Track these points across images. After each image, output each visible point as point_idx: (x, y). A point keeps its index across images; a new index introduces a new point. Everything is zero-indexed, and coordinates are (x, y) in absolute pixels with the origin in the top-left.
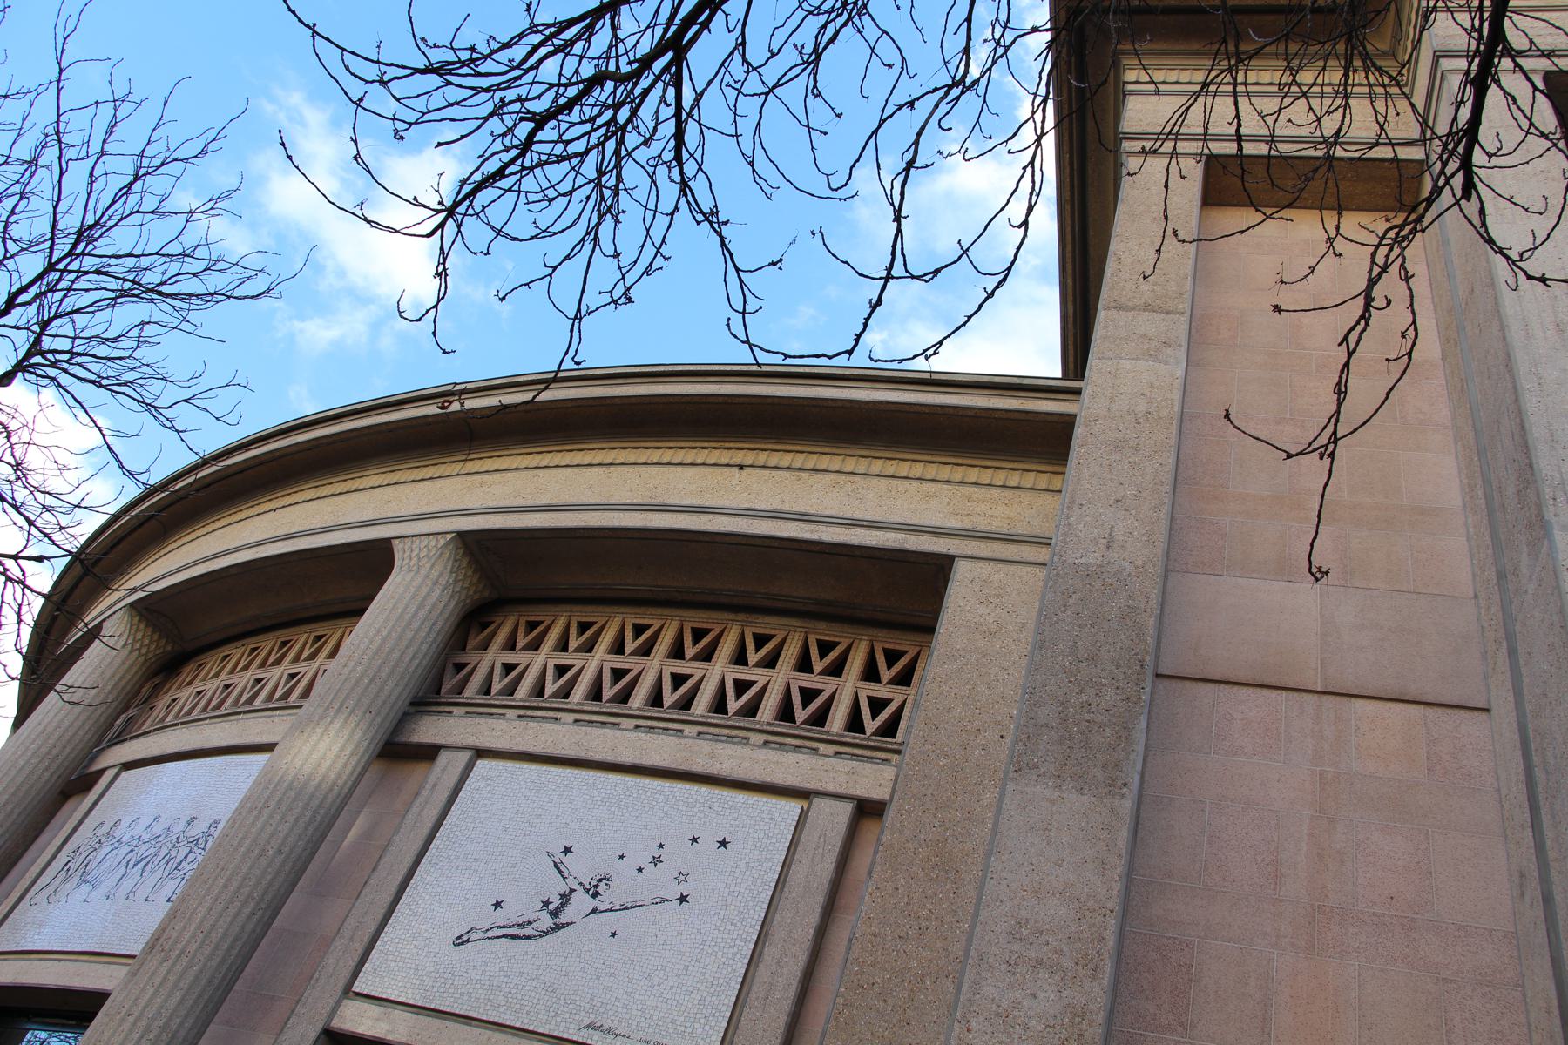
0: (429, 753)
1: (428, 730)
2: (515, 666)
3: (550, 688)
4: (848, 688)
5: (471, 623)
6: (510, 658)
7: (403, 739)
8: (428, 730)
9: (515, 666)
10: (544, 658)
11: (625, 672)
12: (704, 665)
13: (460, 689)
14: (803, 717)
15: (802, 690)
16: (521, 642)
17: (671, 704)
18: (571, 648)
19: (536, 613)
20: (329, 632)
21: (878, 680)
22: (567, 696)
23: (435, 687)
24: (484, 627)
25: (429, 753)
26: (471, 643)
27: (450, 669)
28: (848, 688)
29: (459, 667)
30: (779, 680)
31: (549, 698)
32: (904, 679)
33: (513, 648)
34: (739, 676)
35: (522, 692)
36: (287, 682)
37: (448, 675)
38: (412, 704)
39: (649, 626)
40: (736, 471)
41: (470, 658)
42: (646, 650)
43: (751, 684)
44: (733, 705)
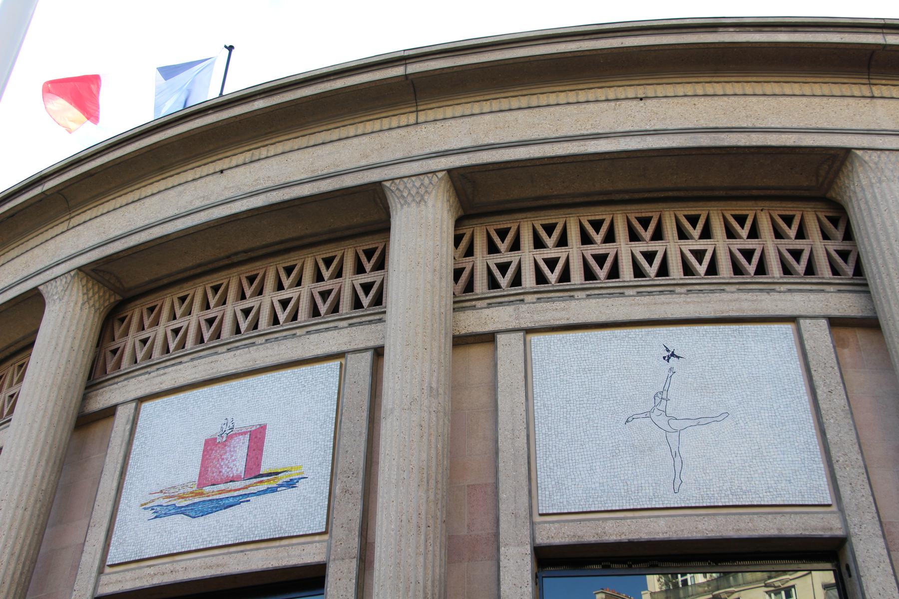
0: (110, 412)
1: (103, 399)
2: (147, 339)
3: (243, 326)
4: (350, 281)
5: (111, 321)
6: (175, 324)
7: (86, 411)
8: (103, 399)
9: (147, 339)
10: (165, 327)
11: (329, 292)
12: (188, 317)
13: (118, 366)
14: (327, 307)
15: (281, 302)
16: (147, 323)
17: (249, 328)
18: (212, 305)
19: (149, 301)
20: (191, 292)
21: (365, 272)
22: (219, 337)
23: (99, 368)
24: (122, 320)
25: (110, 412)
26: (117, 334)
27: (109, 354)
28: (350, 281)
29: (114, 352)
30: (304, 294)
31: (176, 348)
32: (381, 265)
33: (208, 307)
34: (363, 281)
35: (156, 353)
36: (9, 402)
37: (138, 351)
38: (86, 388)
39: (187, 295)
40: (219, 175)
41: (118, 343)
42: (339, 274)
43: (289, 300)
44: (323, 309)
